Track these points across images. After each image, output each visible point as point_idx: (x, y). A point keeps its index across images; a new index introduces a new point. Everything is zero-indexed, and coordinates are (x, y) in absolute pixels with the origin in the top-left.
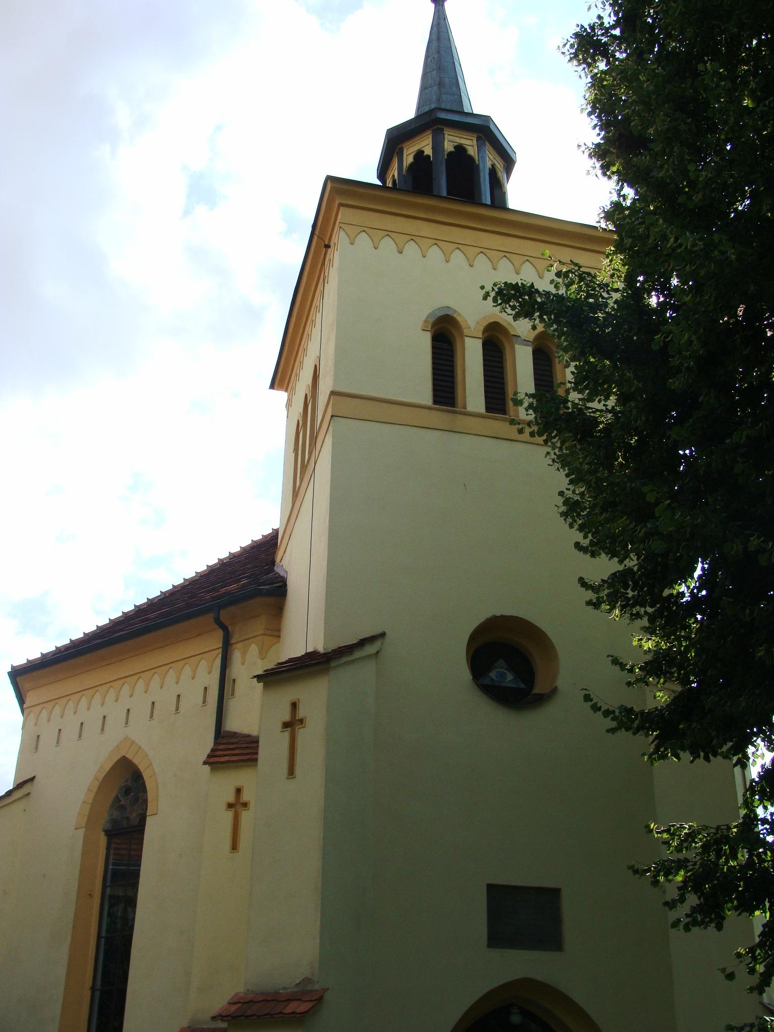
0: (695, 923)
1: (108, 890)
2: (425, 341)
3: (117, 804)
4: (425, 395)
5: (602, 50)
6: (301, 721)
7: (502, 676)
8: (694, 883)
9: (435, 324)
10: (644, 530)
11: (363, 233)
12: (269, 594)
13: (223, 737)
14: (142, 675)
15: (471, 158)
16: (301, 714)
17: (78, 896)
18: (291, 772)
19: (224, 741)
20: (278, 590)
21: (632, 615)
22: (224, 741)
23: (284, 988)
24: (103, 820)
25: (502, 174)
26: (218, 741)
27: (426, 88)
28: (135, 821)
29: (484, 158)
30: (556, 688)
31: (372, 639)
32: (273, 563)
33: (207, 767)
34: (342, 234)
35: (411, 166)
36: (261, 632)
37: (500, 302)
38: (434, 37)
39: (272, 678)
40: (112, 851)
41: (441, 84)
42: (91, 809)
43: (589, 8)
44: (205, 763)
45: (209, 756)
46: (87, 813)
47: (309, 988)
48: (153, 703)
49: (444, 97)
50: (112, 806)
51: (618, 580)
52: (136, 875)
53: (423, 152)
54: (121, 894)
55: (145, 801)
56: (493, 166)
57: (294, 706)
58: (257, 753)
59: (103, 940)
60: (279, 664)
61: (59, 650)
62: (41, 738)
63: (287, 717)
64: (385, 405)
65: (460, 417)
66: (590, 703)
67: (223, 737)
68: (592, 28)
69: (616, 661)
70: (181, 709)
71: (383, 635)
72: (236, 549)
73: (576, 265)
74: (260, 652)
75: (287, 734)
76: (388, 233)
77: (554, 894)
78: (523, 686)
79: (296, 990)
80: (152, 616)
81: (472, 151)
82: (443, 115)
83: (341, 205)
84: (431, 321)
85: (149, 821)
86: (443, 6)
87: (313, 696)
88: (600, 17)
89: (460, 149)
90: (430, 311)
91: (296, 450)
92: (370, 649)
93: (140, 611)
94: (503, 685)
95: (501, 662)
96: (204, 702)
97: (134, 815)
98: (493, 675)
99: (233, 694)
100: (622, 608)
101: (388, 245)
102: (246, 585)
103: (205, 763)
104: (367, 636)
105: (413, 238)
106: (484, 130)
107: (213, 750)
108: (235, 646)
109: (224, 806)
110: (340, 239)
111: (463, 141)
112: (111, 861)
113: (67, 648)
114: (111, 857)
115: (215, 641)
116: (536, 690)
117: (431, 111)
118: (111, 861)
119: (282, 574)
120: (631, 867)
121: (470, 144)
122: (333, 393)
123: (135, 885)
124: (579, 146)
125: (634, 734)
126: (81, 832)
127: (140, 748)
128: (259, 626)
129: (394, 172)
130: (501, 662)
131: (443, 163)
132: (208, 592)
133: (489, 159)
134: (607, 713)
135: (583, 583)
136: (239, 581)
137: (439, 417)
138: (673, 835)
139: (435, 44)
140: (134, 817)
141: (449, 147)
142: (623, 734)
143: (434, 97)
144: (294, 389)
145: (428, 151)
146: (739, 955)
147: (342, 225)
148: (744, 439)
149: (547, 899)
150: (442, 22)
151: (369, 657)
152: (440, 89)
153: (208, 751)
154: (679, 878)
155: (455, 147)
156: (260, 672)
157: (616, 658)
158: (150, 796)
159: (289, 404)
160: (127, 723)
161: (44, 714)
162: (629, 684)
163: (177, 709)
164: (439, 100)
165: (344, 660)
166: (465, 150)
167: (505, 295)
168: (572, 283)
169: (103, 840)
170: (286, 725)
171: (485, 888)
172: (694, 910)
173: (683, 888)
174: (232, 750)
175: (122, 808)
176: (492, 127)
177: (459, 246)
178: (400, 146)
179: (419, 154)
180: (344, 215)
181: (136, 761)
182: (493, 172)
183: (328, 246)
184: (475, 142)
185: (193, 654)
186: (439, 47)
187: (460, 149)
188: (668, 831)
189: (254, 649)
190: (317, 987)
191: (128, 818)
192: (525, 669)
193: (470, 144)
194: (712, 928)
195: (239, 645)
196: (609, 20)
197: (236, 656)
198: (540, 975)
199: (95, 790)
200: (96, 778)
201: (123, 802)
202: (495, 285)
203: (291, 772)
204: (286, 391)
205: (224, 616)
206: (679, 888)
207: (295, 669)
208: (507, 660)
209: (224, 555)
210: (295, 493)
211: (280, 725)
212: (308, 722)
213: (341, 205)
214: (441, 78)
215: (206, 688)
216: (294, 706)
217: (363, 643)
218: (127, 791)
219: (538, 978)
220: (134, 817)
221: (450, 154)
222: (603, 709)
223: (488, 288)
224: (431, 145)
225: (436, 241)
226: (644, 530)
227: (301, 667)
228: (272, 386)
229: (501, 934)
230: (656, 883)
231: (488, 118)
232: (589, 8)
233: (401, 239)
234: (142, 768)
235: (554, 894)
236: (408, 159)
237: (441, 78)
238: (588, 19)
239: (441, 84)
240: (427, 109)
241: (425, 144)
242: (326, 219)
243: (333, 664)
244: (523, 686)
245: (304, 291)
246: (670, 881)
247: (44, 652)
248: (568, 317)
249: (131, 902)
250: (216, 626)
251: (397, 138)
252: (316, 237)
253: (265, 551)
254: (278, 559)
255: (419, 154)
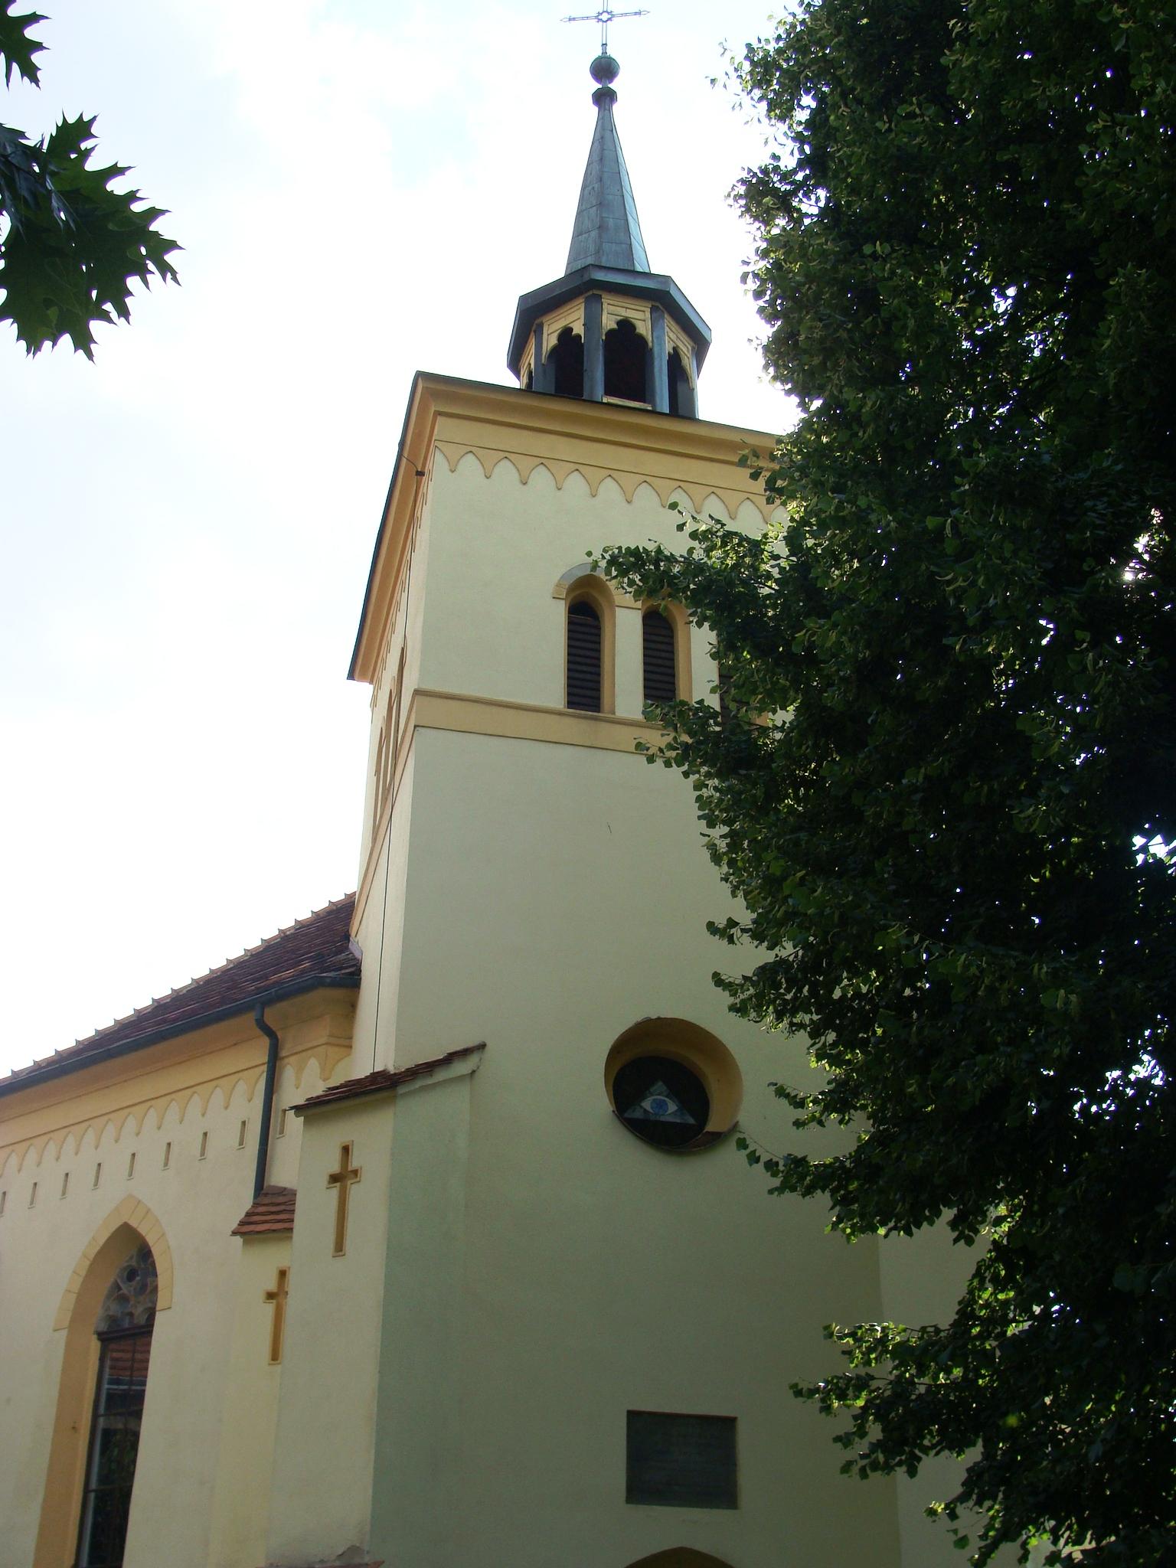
0: (875, 1466)
1: (101, 1420)
2: (557, 616)
3: (117, 1295)
4: (554, 691)
5: (784, 204)
6: (355, 1172)
7: (661, 1105)
8: (879, 1409)
9: (572, 588)
10: (783, 908)
11: (470, 455)
12: (335, 984)
13: (266, 1195)
14: (173, 1096)
15: (642, 339)
16: (354, 1163)
17: (56, 1431)
18: (339, 1247)
19: (266, 1200)
20: (350, 978)
21: (792, 1024)
22: (266, 1200)
23: (322, 1561)
24: (96, 1319)
25: (688, 362)
26: (259, 1200)
27: (581, 234)
28: (142, 1320)
29: (661, 339)
30: (736, 1125)
31: (465, 1053)
32: (347, 937)
33: (238, 1240)
34: (438, 453)
35: (555, 349)
36: (323, 1040)
37: (614, 573)
38: (596, 158)
39: (314, 1109)
40: (108, 1363)
41: (602, 228)
42: (78, 1301)
43: (766, 142)
44: (234, 1233)
45: (242, 1223)
46: (72, 1307)
47: (357, 1560)
48: (169, 1144)
49: (606, 246)
50: (108, 1297)
51: (767, 975)
52: (139, 1397)
53: (571, 329)
54: (120, 1426)
55: (155, 1289)
56: (674, 349)
57: (346, 1150)
58: (292, 1221)
59: (92, 1496)
60: (330, 1089)
61: (38, 1066)
62: (40, 1190)
63: (336, 1168)
64: (494, 709)
65: (604, 725)
66: (745, 1152)
67: (266, 1195)
68: (765, 171)
69: (781, 1092)
70: (210, 1153)
71: (482, 1047)
72: (305, 915)
73: (718, 522)
74: (323, 1069)
75: (335, 1192)
76: (507, 454)
77: (725, 1425)
78: (691, 1121)
79: (338, 1563)
80: (172, 1015)
81: (643, 328)
82: (600, 276)
83: (441, 414)
84: (567, 584)
85: (160, 1319)
86: (610, 110)
87: (373, 1135)
88: (775, 157)
89: (626, 326)
90: (564, 570)
91: (378, 772)
92: (461, 1068)
93: (160, 1008)
94: (662, 1119)
95: (660, 1086)
96: (241, 1143)
97: (140, 1309)
98: (647, 1104)
99: (282, 1132)
100: (779, 1017)
101: (505, 472)
102: (313, 964)
103: (234, 1233)
104: (458, 1049)
105: (543, 461)
106: (663, 298)
107: (248, 1215)
108: (286, 1061)
109: (262, 1296)
110: (438, 465)
111: (630, 314)
112: (106, 1376)
113: (50, 1062)
114: (107, 1370)
115: (258, 1053)
116: (710, 1127)
117: (585, 268)
118: (106, 1376)
119: (357, 954)
120: (794, 1387)
121: (641, 317)
122: (417, 692)
123: (138, 1415)
124: (750, 340)
125: (804, 1196)
126: (63, 1334)
127: (148, 1211)
128: (321, 1032)
129: (529, 359)
130: (660, 1086)
131: (598, 350)
132: (254, 980)
133: (667, 339)
134: (771, 1166)
135: (718, 980)
136: (299, 963)
137: (576, 726)
138: (858, 1340)
139: (596, 166)
140: (139, 1311)
141: (609, 322)
142: (792, 1198)
143: (592, 248)
144: (380, 680)
145: (578, 329)
146: (932, 1512)
147: (438, 444)
148: (921, 779)
149: (716, 1434)
150: (608, 134)
151: (460, 1078)
152: (600, 237)
153: (241, 1215)
154: (860, 1403)
155: (619, 323)
156: (301, 1101)
157: (782, 1087)
158: (162, 1281)
159: (374, 703)
160: (130, 1174)
161: (14, 1160)
162: (798, 1124)
163: (203, 1153)
164: (598, 251)
165: (418, 1084)
166: (633, 327)
167: (621, 564)
168: (712, 548)
169: (95, 1345)
170: (334, 1179)
171: (732, 1415)
172: (875, 1447)
173: (861, 1416)
174: (269, 1214)
175: (123, 1299)
176: (673, 292)
177: (611, 472)
178: (538, 321)
179: (566, 334)
180: (444, 428)
181: (143, 1230)
182: (675, 359)
183: (421, 474)
184: (648, 315)
185: (225, 1072)
186: (602, 171)
187: (626, 326)
188: (853, 1335)
189: (313, 1065)
190: (367, 1559)
191: (131, 1314)
192: (694, 1094)
193: (641, 317)
194: (901, 1472)
195: (292, 1059)
196: (789, 162)
197: (288, 1074)
198: (702, 1544)
199: (83, 1273)
200: (85, 1256)
201: (125, 1291)
202: (605, 550)
203: (339, 1247)
204: (371, 682)
205: (271, 1016)
206: (855, 1418)
207: (347, 1097)
208: (662, 1085)
209: (288, 923)
210: (374, 840)
211: (325, 1179)
212: (365, 1176)
213: (441, 414)
214: (602, 218)
215: (244, 1123)
216: (346, 1150)
217: (450, 1059)
218: (131, 1274)
219: (700, 1547)
220: (139, 1311)
221: (610, 333)
222: (763, 1159)
223: (597, 555)
224: (582, 321)
225: (578, 467)
226: (783, 908)
227: (357, 1095)
228: (351, 676)
229: (644, 1487)
230: (827, 1409)
231: (667, 279)
232: (766, 142)
233: (525, 463)
234: (151, 1240)
235: (725, 1425)
236: (550, 340)
237: (602, 218)
238: (759, 159)
239: (602, 228)
240: (579, 265)
241: (574, 317)
242: (418, 435)
243: (402, 1090)
244: (691, 1121)
245: (391, 539)
246: (848, 1407)
247: (16, 1069)
248: (718, 590)
249: (132, 1440)
250: (258, 1032)
251: (534, 310)
252: (404, 461)
253: (336, 922)
254: (353, 934)
255: (566, 334)
